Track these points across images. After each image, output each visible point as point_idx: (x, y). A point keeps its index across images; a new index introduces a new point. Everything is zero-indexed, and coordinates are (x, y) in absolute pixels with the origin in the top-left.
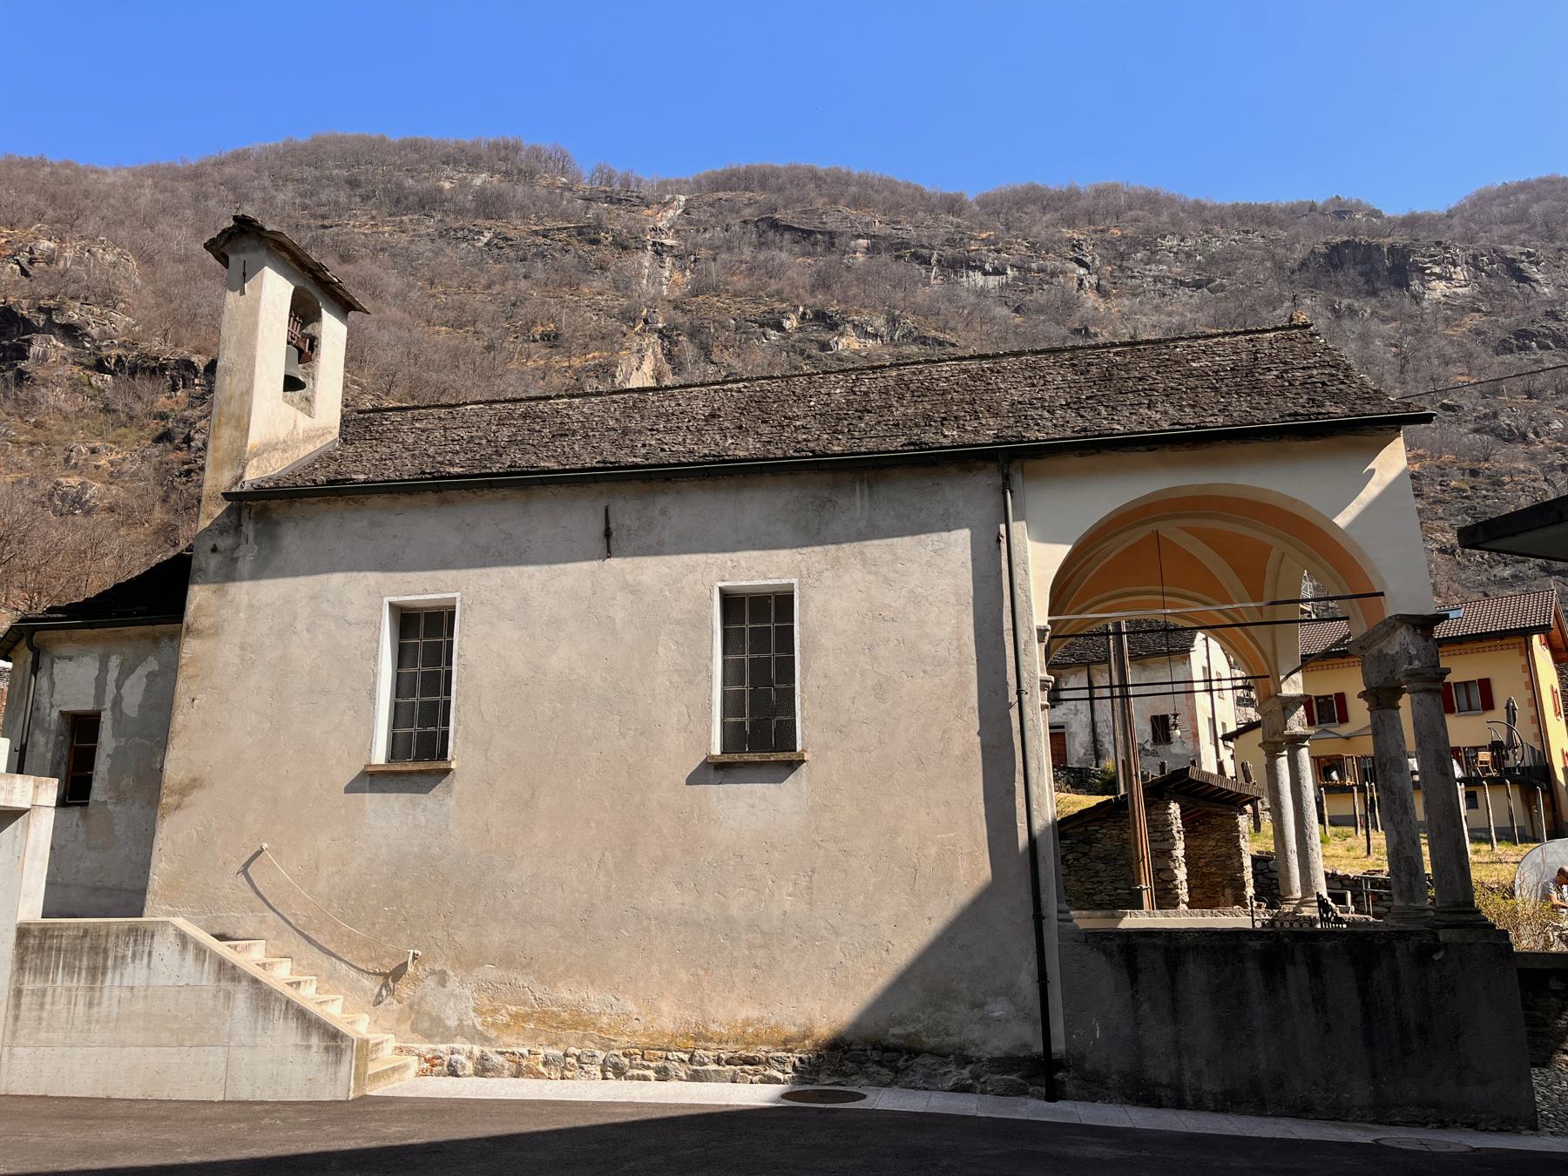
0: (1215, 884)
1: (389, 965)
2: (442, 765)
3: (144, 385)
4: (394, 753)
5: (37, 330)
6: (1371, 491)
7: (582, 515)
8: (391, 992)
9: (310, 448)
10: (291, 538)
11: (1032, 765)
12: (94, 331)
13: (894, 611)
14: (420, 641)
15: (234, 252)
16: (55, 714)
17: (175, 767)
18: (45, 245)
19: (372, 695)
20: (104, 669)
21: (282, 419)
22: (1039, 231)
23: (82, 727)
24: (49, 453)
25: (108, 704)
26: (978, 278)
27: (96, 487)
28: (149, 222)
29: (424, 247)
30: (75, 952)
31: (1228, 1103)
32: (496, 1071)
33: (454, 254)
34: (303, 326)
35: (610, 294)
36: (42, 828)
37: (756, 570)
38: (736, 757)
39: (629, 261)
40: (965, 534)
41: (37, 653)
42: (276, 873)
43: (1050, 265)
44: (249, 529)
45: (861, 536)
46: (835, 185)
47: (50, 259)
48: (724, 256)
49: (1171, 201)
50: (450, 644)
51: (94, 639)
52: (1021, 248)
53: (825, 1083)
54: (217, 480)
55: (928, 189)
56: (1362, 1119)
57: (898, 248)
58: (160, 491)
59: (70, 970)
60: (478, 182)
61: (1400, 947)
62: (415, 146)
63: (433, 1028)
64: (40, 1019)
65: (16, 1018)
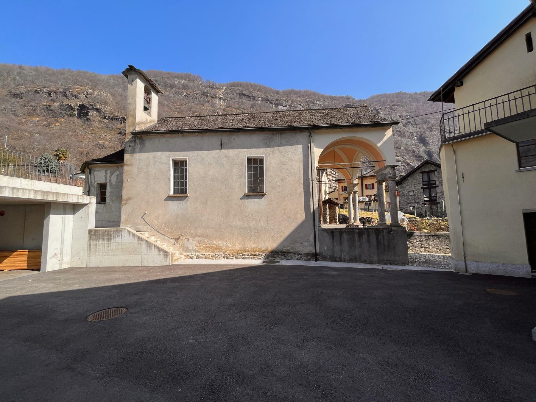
0: (332, 220)
1: (176, 237)
2: (186, 195)
3: (115, 122)
4: (175, 192)
5: (90, 109)
6: (385, 139)
7: (215, 139)
8: (177, 242)
9: (151, 124)
10: (148, 143)
11: (314, 195)
12: (103, 110)
13: (285, 162)
14: (179, 168)
15: (130, 75)
16: (96, 183)
17: (125, 194)
18: (90, 91)
19: (169, 179)
20: (106, 173)
21: (145, 115)
22: (294, 98)
23: (103, 187)
24: (96, 136)
25: (108, 181)
26: (282, 107)
27: (106, 143)
28: (113, 87)
29: (171, 95)
30: (103, 235)
31: (350, 261)
32: (201, 258)
33: (178, 97)
34: (148, 95)
35: (210, 107)
36: (93, 208)
37: (255, 153)
38: (251, 194)
39: (214, 100)
40: (301, 146)
41: (90, 170)
42: (150, 218)
43: (295, 105)
44: (138, 141)
45: (279, 146)
46: (255, 87)
47: (91, 94)
48: (233, 100)
49: (318, 94)
50: (186, 169)
51: (103, 167)
52: (290, 102)
53: (270, 259)
54: (129, 130)
55: (273, 89)
56: (376, 263)
57: (267, 100)
58: (120, 144)
59: (103, 239)
60: (182, 82)
61: (384, 230)
62: (169, 74)
63: (187, 250)
64: (96, 250)
65: (90, 250)
